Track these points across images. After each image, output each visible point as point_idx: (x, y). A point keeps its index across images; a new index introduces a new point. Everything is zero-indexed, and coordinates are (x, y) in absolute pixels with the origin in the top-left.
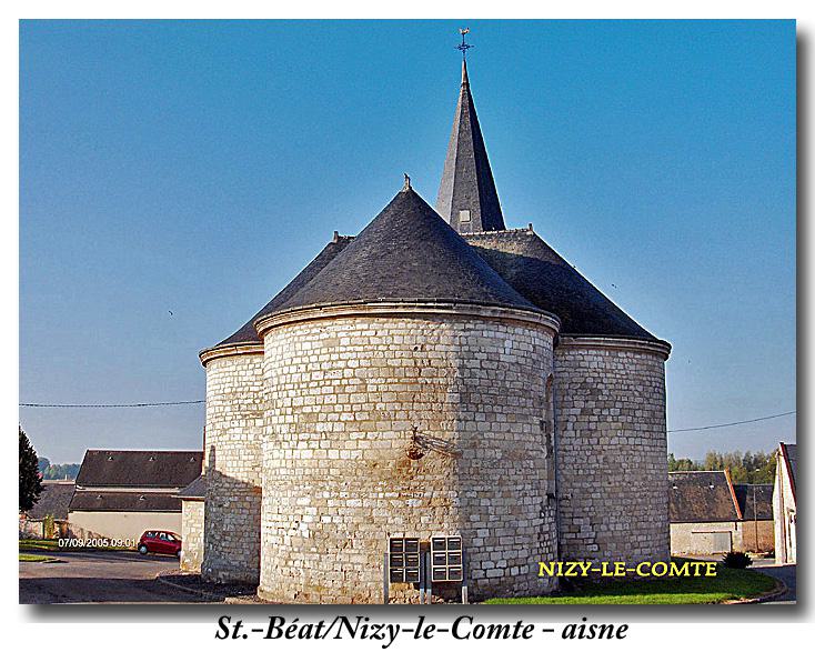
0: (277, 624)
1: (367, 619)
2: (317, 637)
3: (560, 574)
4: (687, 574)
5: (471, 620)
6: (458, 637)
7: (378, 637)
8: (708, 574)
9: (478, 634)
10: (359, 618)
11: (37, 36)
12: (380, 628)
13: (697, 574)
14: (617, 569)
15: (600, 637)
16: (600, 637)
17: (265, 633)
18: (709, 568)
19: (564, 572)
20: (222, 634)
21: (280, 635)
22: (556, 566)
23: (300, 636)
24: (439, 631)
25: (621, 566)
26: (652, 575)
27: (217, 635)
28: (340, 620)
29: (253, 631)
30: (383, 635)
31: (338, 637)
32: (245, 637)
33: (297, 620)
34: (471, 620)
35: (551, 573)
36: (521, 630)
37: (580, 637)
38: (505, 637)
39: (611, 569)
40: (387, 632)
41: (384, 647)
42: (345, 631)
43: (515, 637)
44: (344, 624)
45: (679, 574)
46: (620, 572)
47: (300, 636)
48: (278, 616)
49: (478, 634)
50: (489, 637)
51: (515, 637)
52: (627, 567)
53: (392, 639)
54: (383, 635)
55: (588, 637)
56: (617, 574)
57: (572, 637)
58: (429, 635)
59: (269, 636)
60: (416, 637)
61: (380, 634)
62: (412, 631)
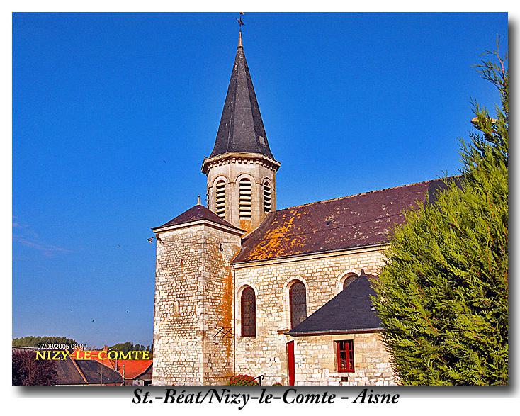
0: (171, 394)
1: (229, 391)
2: (197, 402)
3: (49, 358)
4: (130, 358)
5: (295, 391)
6: (287, 402)
7: (236, 402)
8: (144, 358)
9: (299, 400)
10: (224, 390)
11: (24, 23)
12: (237, 396)
13: (136, 358)
14: (86, 355)
15: (382, 402)
16: (382, 402)
17: (164, 400)
18: (144, 355)
19: (51, 357)
20: (136, 400)
21: (173, 401)
22: (47, 354)
23: (186, 402)
24: (275, 398)
25: (88, 353)
26: (97, 357)
27: (133, 401)
28: (212, 391)
29: (156, 398)
30: (239, 401)
31: (210, 402)
32: (151, 402)
33: (184, 391)
34: (295, 391)
35: (43, 358)
36: (327, 399)
37: (369, 402)
38: (317, 402)
39: (82, 355)
40: (242, 399)
41: (240, 409)
42: (215, 399)
43: (323, 402)
44: (214, 395)
45: (125, 358)
46: (87, 357)
47: (186, 402)
48: (171, 393)
49: (299, 400)
50: (306, 402)
51: (323, 402)
52: (91, 354)
53: (245, 403)
54: (239, 401)
55: (374, 402)
56: (86, 358)
57: (191, 402)
58: (268, 401)
59: (166, 402)
60: (260, 402)
61: (237, 400)
62: (257, 398)
